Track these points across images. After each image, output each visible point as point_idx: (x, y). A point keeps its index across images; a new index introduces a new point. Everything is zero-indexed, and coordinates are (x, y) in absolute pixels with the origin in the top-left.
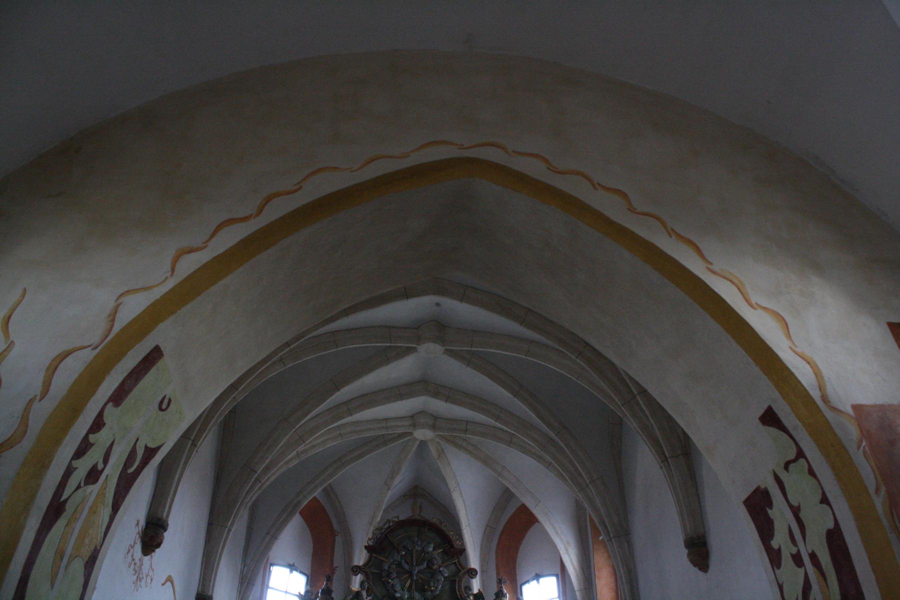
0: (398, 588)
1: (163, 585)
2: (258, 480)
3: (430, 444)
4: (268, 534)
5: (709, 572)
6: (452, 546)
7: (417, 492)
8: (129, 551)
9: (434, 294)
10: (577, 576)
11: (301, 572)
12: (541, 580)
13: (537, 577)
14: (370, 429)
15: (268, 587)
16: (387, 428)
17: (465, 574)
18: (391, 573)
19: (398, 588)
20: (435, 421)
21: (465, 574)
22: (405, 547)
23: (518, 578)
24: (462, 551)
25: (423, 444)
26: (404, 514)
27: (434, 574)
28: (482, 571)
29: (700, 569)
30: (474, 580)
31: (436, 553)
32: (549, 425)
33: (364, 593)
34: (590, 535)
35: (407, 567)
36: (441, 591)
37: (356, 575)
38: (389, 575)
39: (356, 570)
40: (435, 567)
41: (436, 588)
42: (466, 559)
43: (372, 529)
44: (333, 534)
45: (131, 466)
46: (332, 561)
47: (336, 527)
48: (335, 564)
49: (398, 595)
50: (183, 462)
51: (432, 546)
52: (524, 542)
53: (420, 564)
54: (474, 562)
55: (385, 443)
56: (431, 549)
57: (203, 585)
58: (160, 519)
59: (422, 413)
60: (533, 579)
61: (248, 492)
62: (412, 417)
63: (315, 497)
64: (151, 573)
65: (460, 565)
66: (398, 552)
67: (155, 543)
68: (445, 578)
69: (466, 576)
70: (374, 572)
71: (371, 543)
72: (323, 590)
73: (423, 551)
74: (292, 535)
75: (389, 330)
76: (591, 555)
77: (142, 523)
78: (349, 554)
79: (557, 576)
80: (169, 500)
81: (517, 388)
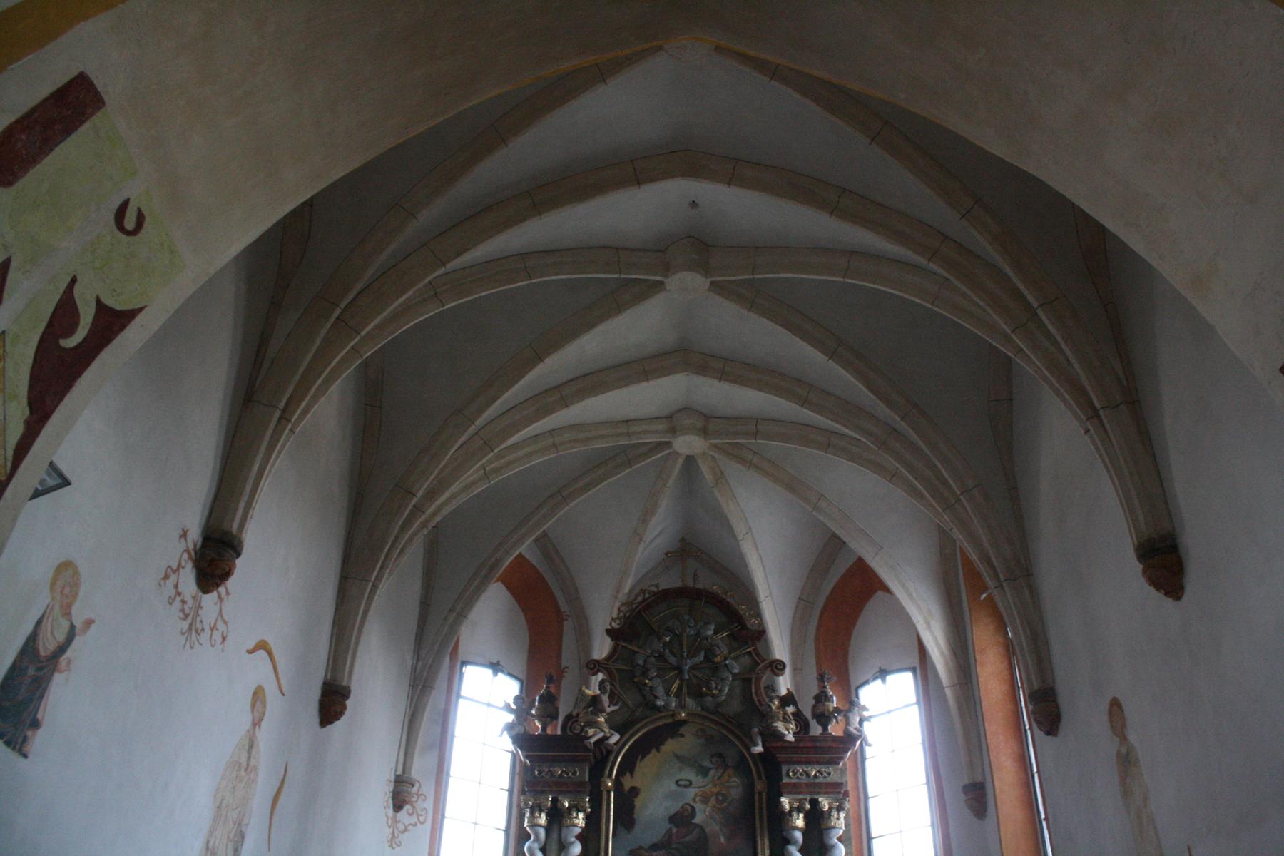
0: (660, 691)
1: (250, 652)
2: (418, 509)
3: (699, 461)
4: (452, 610)
5: (1185, 598)
7: (686, 550)
8: (166, 577)
9: (683, 175)
10: (946, 664)
11: (510, 675)
12: (890, 678)
13: (883, 673)
14: (603, 437)
15: (459, 696)
16: (660, 718)
19: (660, 691)
20: (707, 423)
22: (669, 630)
24: (761, 633)
25: (690, 460)
26: (669, 582)
28: (794, 664)
29: (1166, 594)
30: (781, 678)
32: (889, 403)
34: (964, 598)
35: (672, 660)
36: (729, 695)
37: (595, 674)
38: (645, 672)
39: (595, 666)
40: (718, 659)
41: (720, 691)
43: (618, 604)
44: (560, 617)
45: (70, 332)
46: (559, 656)
47: (564, 606)
48: (564, 664)
49: (660, 703)
50: (267, 438)
51: (713, 627)
53: (694, 656)
54: (780, 647)
55: (629, 463)
56: (710, 632)
57: (334, 670)
58: (227, 533)
59: (686, 410)
60: (875, 678)
61: (404, 528)
62: (670, 417)
63: (520, 555)
64: (221, 626)
65: (758, 654)
67: (219, 572)
68: (734, 675)
69: (768, 673)
70: (622, 671)
72: (542, 697)
73: (698, 634)
74: (491, 612)
75: (613, 253)
76: (968, 628)
77: (195, 535)
79: (913, 670)
80: (242, 505)
81: (835, 347)
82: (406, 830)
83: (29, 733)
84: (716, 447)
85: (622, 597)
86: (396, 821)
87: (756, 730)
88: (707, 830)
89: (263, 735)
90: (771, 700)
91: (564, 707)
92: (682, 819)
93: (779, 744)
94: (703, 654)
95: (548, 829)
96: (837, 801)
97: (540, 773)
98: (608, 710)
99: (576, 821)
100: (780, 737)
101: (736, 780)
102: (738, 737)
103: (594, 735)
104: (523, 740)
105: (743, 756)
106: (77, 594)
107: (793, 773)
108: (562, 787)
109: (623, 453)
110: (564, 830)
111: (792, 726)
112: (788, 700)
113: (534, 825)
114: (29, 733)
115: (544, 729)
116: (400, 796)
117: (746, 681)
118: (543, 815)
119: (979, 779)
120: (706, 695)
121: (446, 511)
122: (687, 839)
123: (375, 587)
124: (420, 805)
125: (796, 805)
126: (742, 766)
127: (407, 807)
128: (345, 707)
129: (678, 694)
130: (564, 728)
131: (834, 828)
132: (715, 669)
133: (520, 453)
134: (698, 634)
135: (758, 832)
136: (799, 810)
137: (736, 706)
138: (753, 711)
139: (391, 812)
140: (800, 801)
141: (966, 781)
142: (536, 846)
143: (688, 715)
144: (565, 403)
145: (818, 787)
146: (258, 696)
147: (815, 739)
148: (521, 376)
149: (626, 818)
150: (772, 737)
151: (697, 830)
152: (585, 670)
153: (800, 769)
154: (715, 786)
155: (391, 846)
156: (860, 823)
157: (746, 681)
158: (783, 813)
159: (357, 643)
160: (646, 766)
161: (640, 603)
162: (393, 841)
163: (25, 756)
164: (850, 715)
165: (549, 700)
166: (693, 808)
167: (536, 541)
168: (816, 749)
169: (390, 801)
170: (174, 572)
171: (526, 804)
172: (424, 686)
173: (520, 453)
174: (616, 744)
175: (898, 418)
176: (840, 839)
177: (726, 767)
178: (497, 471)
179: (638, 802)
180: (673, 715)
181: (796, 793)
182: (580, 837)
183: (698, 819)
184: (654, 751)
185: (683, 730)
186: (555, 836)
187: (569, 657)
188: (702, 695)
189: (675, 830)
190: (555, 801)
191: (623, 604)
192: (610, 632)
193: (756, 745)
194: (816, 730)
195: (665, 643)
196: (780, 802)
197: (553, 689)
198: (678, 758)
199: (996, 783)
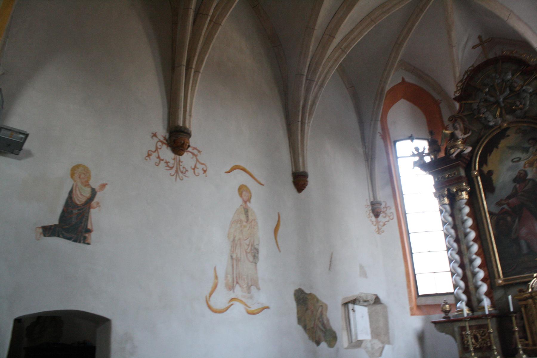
0: (490, 118)
4: (372, 120)
6: (528, 65)
7: (485, 42)
8: (149, 155)
15: (397, 158)
16: (493, 131)
19: (490, 118)
35: (492, 99)
41: (524, 105)
44: (437, 103)
47: (437, 97)
49: (491, 124)
53: (504, 92)
56: (509, 77)
61: (308, 91)
68: (530, 93)
71: (457, 95)
73: (503, 81)
74: (400, 113)
82: (384, 225)
83: (87, 235)
86: (378, 222)
89: (253, 205)
92: (520, 178)
94: (508, 89)
106: (90, 176)
114: (87, 235)
122: (526, 188)
124: (388, 212)
127: (381, 215)
128: (307, 181)
129: (501, 115)
130: (446, 153)
132: (518, 95)
134: (503, 81)
139: (374, 219)
143: (508, 124)
146: (242, 189)
149: (489, 188)
159: (303, 151)
160: (493, 158)
162: (379, 231)
163: (89, 244)
166: (525, 172)
169: (372, 214)
170: (155, 152)
172: (372, 159)
173: (356, 33)
179: (494, 177)
180: (500, 127)
183: (529, 176)
184: (495, 149)
185: (508, 133)
188: (515, 111)
189: (518, 186)
190: (448, 190)
191: (459, 82)
195: (487, 93)
198: (509, 148)
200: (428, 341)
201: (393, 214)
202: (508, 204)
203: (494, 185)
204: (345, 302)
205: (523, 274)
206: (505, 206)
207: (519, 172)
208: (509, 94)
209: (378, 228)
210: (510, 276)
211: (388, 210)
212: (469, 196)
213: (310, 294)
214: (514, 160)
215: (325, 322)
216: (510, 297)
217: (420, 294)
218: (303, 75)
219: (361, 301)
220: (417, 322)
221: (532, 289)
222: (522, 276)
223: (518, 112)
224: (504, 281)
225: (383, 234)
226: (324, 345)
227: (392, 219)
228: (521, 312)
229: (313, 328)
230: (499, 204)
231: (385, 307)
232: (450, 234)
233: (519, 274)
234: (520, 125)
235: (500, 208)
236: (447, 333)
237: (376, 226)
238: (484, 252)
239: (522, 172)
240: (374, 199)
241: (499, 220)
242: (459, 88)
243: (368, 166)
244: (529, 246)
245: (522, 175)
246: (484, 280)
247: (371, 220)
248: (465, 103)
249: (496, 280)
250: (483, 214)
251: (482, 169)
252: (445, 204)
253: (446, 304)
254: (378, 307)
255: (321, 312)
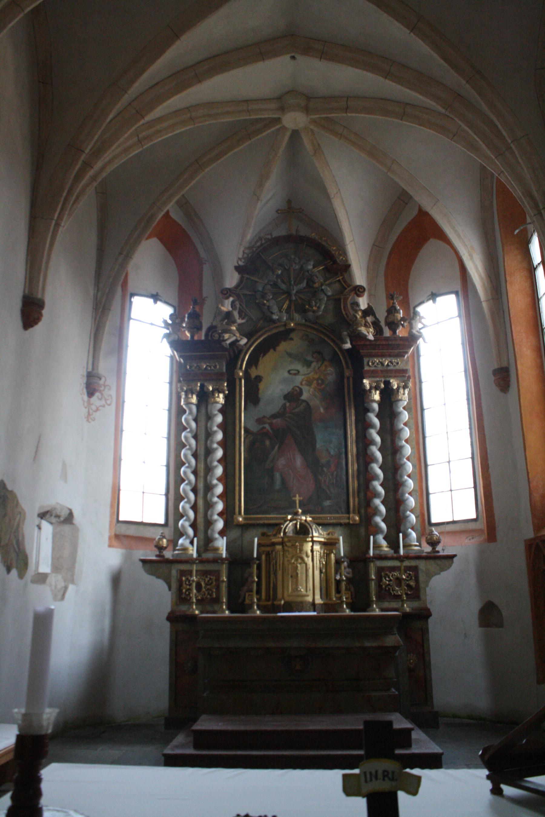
0: (275, 309)
2: (87, 165)
4: (120, 254)
6: (335, 262)
7: (290, 210)
10: (484, 285)
12: (439, 299)
13: (433, 296)
14: (228, 113)
15: (130, 318)
16: (277, 327)
17: (351, 291)
18: (266, 294)
19: (275, 309)
20: (308, 101)
21: (351, 291)
22: (280, 265)
23: (411, 300)
24: (347, 267)
25: (295, 134)
27: (313, 292)
28: (370, 290)
31: (316, 270)
33: (236, 314)
35: (283, 287)
36: (325, 311)
37: (228, 298)
38: (263, 297)
39: (226, 293)
40: (316, 285)
41: (319, 308)
42: (351, 277)
48: (205, 294)
49: (275, 317)
51: (312, 263)
52: (417, 260)
54: (359, 277)
56: (310, 267)
60: (428, 300)
62: (279, 98)
65: (345, 282)
66: (273, 272)
68: (328, 297)
70: (247, 294)
71: (240, 263)
73: (302, 269)
74: (148, 258)
78: (218, 274)
79: (457, 293)
82: (97, 410)
84: (314, 122)
85: (246, 243)
86: (89, 404)
87: (345, 333)
88: (311, 404)
90: (356, 311)
91: (206, 322)
92: (293, 396)
93: (362, 343)
94: (305, 281)
95: (198, 406)
96: (403, 382)
97: (191, 367)
98: (240, 321)
99: (218, 399)
100: (364, 337)
101: (330, 370)
102: (333, 341)
103: (228, 338)
104: (177, 344)
105: (336, 354)
107: (371, 363)
108: (206, 376)
109: (245, 128)
110: (209, 407)
111: (371, 330)
112: (369, 312)
113: (188, 403)
115: (192, 337)
116: (92, 385)
117: (337, 301)
118: (195, 397)
119: (505, 364)
120: (309, 310)
121: (109, 169)
122: (296, 410)
123: (57, 225)
124: (106, 392)
125: (374, 384)
126: (335, 360)
127: (97, 394)
128: (41, 315)
129: (288, 311)
130: (207, 335)
131: (401, 400)
133: (165, 124)
135: (347, 404)
136: (376, 388)
137: (330, 318)
138: (344, 321)
139: (86, 397)
140: (377, 382)
141: (496, 367)
142: (190, 417)
143: (295, 324)
144: (199, 79)
145: (388, 373)
147: (387, 339)
148: (162, 51)
149: (253, 397)
150: (357, 337)
151: (304, 404)
152: (221, 296)
153: (377, 360)
154: (316, 373)
155: (88, 420)
156: (416, 399)
157: (337, 301)
158: (364, 390)
159: (47, 267)
161: (258, 247)
162: (89, 417)
164: (413, 322)
165: (195, 317)
166: (301, 390)
167: (178, 202)
168: (388, 346)
169: (85, 390)
171: (182, 389)
173: (165, 124)
174: (245, 344)
175: (464, 82)
176: (404, 408)
177: (324, 360)
178: (149, 138)
179: (262, 386)
180: (285, 325)
181: (373, 377)
182: (221, 411)
183: (304, 397)
184: (272, 351)
185: (293, 335)
186: (203, 411)
187: (208, 290)
189: (288, 404)
190: (202, 386)
191: (246, 248)
192: (237, 268)
193: (346, 343)
194: (387, 333)
195: (278, 276)
196: (362, 383)
197: (197, 309)
198: (290, 355)
199: (519, 367)
200: (124, 585)
201: (112, 398)
202: (271, 424)
203: (260, 396)
204: (42, 511)
205: (269, 514)
206: (267, 426)
207: (293, 389)
208: (304, 288)
209: (89, 412)
210: (253, 514)
211: (106, 390)
212: (225, 402)
213: (12, 492)
214: (291, 372)
215: (20, 538)
216: (256, 540)
217: (121, 519)
218: (83, 152)
219: (54, 515)
220: (114, 557)
221: (285, 533)
222: (268, 516)
223: (310, 314)
224: (244, 519)
225: (93, 423)
226: (14, 572)
227: (109, 405)
228: (218, 580)
229: (7, 545)
230: (260, 421)
231: (76, 530)
232: (190, 445)
233: (263, 514)
234: (309, 330)
235: (261, 427)
236: (158, 577)
237: (87, 410)
238: (228, 479)
239: (297, 389)
240: (93, 369)
241: (255, 441)
242: (245, 255)
243: (95, 319)
244: (283, 481)
245: (295, 393)
246: (220, 514)
247: (83, 398)
248: (247, 279)
249: (235, 516)
250: (237, 429)
251: (249, 370)
252: (192, 403)
253: (164, 537)
254: (66, 528)
255: (20, 519)
